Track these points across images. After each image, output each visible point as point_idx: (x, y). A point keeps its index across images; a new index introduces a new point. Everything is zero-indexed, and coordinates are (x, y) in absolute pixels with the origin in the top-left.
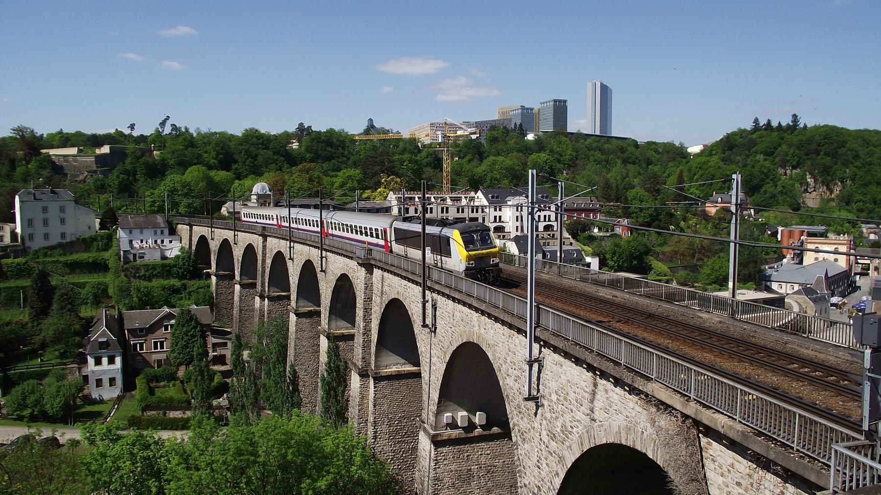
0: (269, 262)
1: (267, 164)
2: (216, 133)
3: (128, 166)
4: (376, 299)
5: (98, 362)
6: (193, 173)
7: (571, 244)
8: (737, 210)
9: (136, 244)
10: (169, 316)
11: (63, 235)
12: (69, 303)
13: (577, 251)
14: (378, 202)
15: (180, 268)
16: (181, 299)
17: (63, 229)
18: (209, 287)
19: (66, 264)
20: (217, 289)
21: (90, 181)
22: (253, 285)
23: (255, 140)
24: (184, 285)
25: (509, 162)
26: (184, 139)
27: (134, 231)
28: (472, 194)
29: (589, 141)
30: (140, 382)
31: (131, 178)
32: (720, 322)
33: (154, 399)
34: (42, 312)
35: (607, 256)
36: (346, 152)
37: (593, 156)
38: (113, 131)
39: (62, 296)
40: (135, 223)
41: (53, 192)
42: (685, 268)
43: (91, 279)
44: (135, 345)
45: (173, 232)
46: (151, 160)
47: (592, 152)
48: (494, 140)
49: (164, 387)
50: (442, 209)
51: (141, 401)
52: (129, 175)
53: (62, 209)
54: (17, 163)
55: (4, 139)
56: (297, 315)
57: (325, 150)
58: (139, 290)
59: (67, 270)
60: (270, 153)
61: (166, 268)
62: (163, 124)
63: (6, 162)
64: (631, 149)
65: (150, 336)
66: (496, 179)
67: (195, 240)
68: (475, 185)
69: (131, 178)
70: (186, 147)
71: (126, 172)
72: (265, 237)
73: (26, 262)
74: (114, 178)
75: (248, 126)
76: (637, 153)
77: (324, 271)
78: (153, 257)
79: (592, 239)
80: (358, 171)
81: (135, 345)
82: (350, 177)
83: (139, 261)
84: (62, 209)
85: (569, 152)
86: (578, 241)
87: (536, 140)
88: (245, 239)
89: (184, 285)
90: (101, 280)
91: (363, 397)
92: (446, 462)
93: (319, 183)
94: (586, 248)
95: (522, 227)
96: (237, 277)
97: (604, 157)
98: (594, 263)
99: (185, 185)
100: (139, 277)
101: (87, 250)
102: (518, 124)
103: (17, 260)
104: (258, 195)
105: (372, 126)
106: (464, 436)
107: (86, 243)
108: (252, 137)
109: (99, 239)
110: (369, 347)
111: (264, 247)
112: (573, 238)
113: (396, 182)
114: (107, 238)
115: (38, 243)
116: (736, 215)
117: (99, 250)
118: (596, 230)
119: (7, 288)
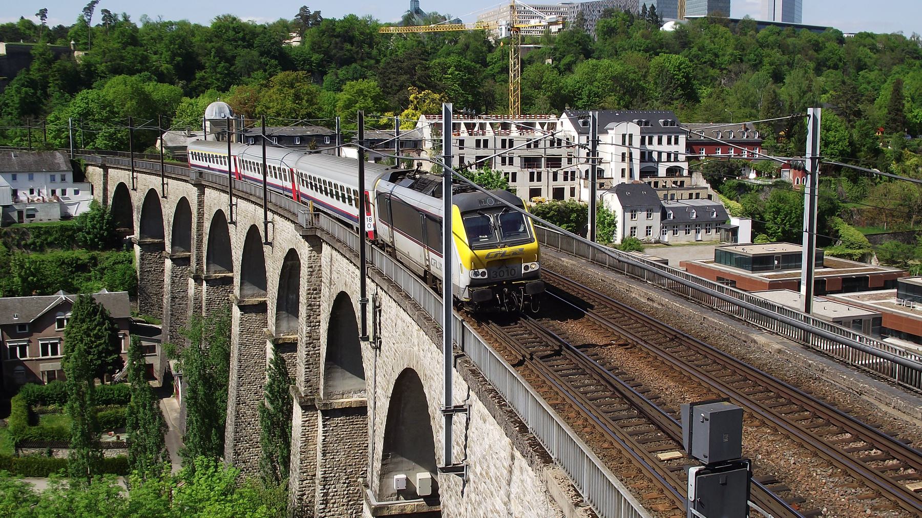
0: (207, 225)
1: (249, 71)
2: (171, 24)
3: (35, 75)
4: (325, 291)
6: (114, 88)
7: (710, 197)
8: (814, 167)
9: (23, 196)
10: (64, 306)
13: (720, 209)
14: (406, 131)
15: (88, 233)
16: (89, 279)
18: (131, 262)
20: (142, 264)
22: (186, 261)
23: (231, 33)
24: (94, 258)
25: (617, 67)
26: (122, 33)
27: (19, 176)
28: (553, 119)
29: (763, 32)
31: (39, 93)
32: (779, 351)
33: (34, 430)
35: (767, 216)
36: (375, 52)
37: (769, 56)
38: (15, 20)
42: (895, 235)
44: (13, 349)
45: (80, 177)
46: (69, 65)
47: (767, 51)
48: (609, 32)
49: (54, 412)
50: (504, 141)
51: (15, 433)
52: (35, 89)
55: (3, 27)
56: (242, 308)
57: (342, 49)
58: (22, 267)
60: (255, 53)
61: (67, 233)
62: (89, 9)
64: (832, 45)
65: (36, 335)
66: (596, 95)
67: (112, 190)
68: (560, 102)
69: (39, 93)
70: (125, 45)
71: (32, 84)
72: (201, 188)
75: (222, 12)
76: (842, 51)
77: (270, 244)
78: (49, 215)
79: (743, 189)
81: (13, 349)
82: (360, 92)
83: (26, 221)
85: (730, 51)
86: (721, 193)
87: (677, 32)
88: (178, 190)
89: (94, 258)
91: (307, 440)
93: (311, 102)
94: (733, 203)
95: (631, 170)
96: (168, 249)
97: (786, 57)
98: (744, 227)
100: (27, 246)
102: (648, 7)
104: (214, 122)
105: (418, 11)
106: (426, 509)
110: (317, 364)
111: (201, 203)
112: (713, 187)
113: (433, 100)
116: (813, 174)
118: (752, 175)
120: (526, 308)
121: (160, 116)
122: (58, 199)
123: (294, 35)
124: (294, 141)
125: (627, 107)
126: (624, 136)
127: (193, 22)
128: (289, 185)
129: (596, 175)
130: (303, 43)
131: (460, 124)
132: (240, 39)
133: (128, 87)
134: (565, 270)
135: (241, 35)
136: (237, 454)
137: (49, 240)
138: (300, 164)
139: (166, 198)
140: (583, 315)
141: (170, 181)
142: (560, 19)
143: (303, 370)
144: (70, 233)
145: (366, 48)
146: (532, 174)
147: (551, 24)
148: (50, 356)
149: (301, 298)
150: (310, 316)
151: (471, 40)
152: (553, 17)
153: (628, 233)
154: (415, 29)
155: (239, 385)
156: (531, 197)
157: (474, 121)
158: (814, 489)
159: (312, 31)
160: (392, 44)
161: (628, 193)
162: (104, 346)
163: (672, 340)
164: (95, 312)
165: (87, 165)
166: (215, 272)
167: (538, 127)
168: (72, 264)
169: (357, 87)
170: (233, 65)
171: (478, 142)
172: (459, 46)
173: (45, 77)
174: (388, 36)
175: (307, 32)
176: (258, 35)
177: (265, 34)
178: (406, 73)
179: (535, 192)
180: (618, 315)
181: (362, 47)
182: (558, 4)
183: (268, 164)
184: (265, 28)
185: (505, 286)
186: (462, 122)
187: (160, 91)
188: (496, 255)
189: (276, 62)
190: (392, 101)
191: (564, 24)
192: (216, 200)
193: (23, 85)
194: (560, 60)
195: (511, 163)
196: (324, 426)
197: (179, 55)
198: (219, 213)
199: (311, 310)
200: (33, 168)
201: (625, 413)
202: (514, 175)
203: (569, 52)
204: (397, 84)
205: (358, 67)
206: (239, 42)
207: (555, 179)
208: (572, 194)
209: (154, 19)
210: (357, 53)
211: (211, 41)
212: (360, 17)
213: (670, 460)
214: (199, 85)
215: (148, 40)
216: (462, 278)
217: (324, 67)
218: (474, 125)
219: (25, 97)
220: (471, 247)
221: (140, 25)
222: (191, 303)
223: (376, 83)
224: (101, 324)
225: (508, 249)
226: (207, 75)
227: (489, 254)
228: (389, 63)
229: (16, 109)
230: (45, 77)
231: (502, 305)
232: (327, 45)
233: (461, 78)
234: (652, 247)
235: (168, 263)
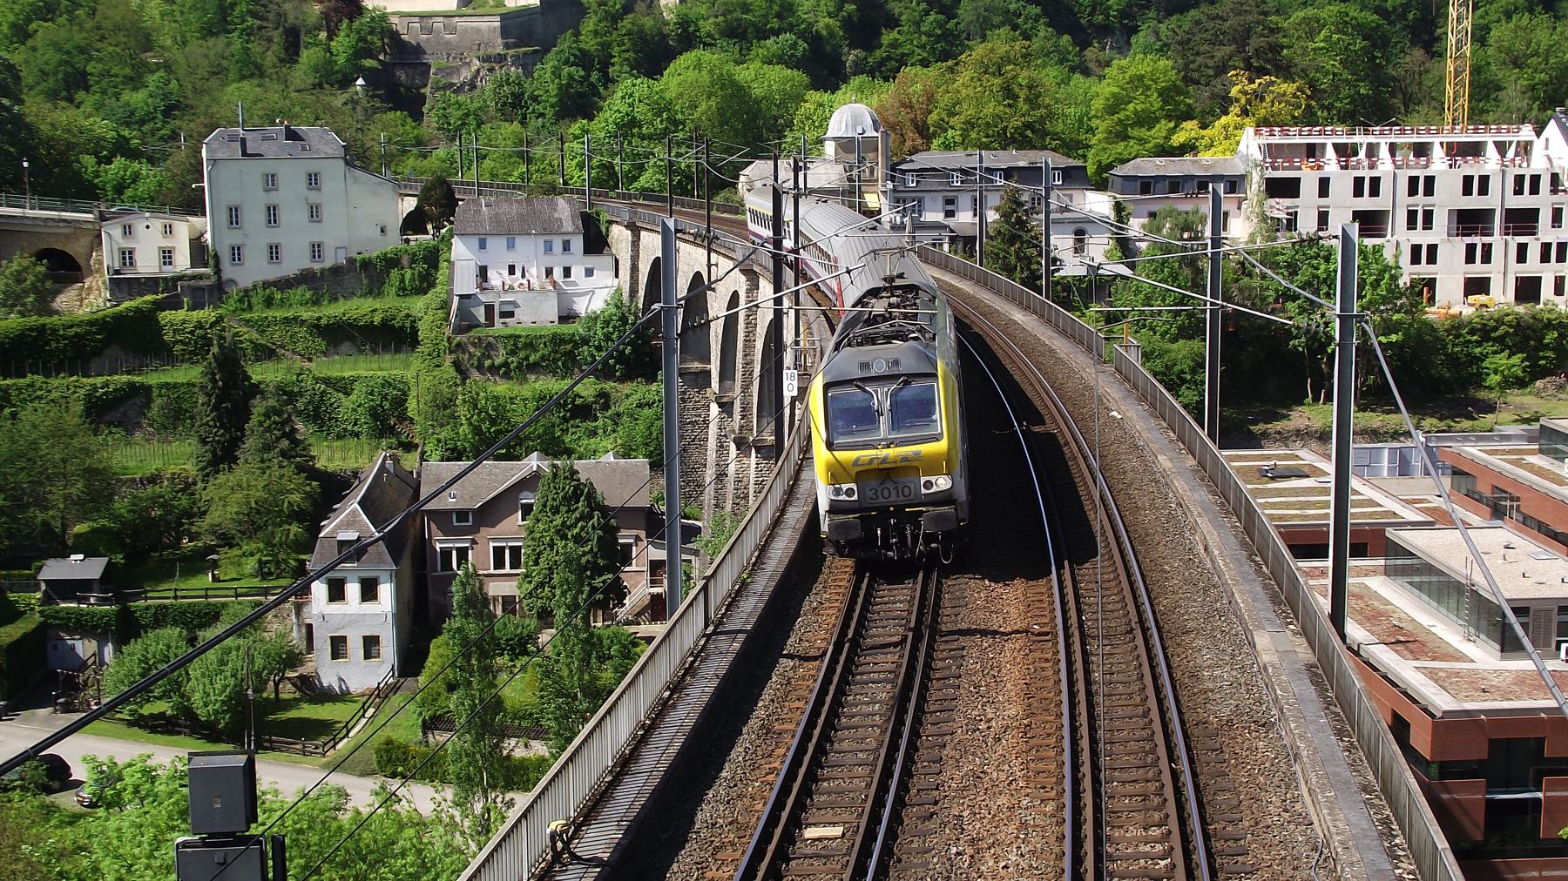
3: (589, 43)
5: (337, 593)
9: (495, 279)
11: (316, 250)
12: (285, 435)
14: (1206, 161)
15: (599, 349)
16: (594, 433)
17: (315, 233)
19: (317, 326)
21: (487, 85)
24: (604, 396)
27: (490, 241)
28: (1527, 132)
30: (440, 651)
31: (595, 76)
34: (222, 456)
39: (267, 415)
40: (496, 219)
41: (292, 135)
43: (368, 370)
44: (446, 554)
45: (596, 243)
46: (648, 22)
50: (1413, 181)
52: (588, 68)
53: (313, 180)
54: (304, 39)
59: (321, 343)
61: (561, 351)
63: (277, 36)
65: (485, 532)
69: (595, 76)
71: (583, 59)
73: (220, 319)
74: (547, 79)
78: (536, 315)
81: (446, 554)
84: (313, 180)
89: (604, 396)
90: (397, 372)
93: (1033, 102)
99: (661, 107)
100: (493, 369)
101: (375, 290)
103: (197, 315)
104: (845, 145)
107: (371, 273)
109: (405, 260)
114: (425, 260)
115: (252, 271)
117: (403, 291)
119: (166, 385)
122: (554, 283)
131: (1324, 145)
133: (705, 73)
137: (532, 359)
144: (569, 347)
146: (1471, 249)
148: (507, 570)
156: (1466, 295)
157: (1357, 139)
162: (589, 557)
164: (576, 496)
165: (610, 222)
167: (1491, 151)
168: (566, 404)
169: (1132, 71)
171: (1358, 182)
173: (606, 46)
179: (1476, 286)
185: (893, 515)
188: (872, 460)
189: (1038, 10)
190: (1197, 97)
193: (567, 62)
195: (1428, 224)
200: (516, 227)
202: (1432, 249)
204: (1211, 63)
213: (820, 839)
214: (889, 58)
217: (1133, 17)
219: (569, 85)
223: (1170, 63)
224: (586, 517)
225: (893, 452)
226: (902, 39)
227: (857, 460)
228: (1198, 23)
229: (552, 106)
230: (606, 46)
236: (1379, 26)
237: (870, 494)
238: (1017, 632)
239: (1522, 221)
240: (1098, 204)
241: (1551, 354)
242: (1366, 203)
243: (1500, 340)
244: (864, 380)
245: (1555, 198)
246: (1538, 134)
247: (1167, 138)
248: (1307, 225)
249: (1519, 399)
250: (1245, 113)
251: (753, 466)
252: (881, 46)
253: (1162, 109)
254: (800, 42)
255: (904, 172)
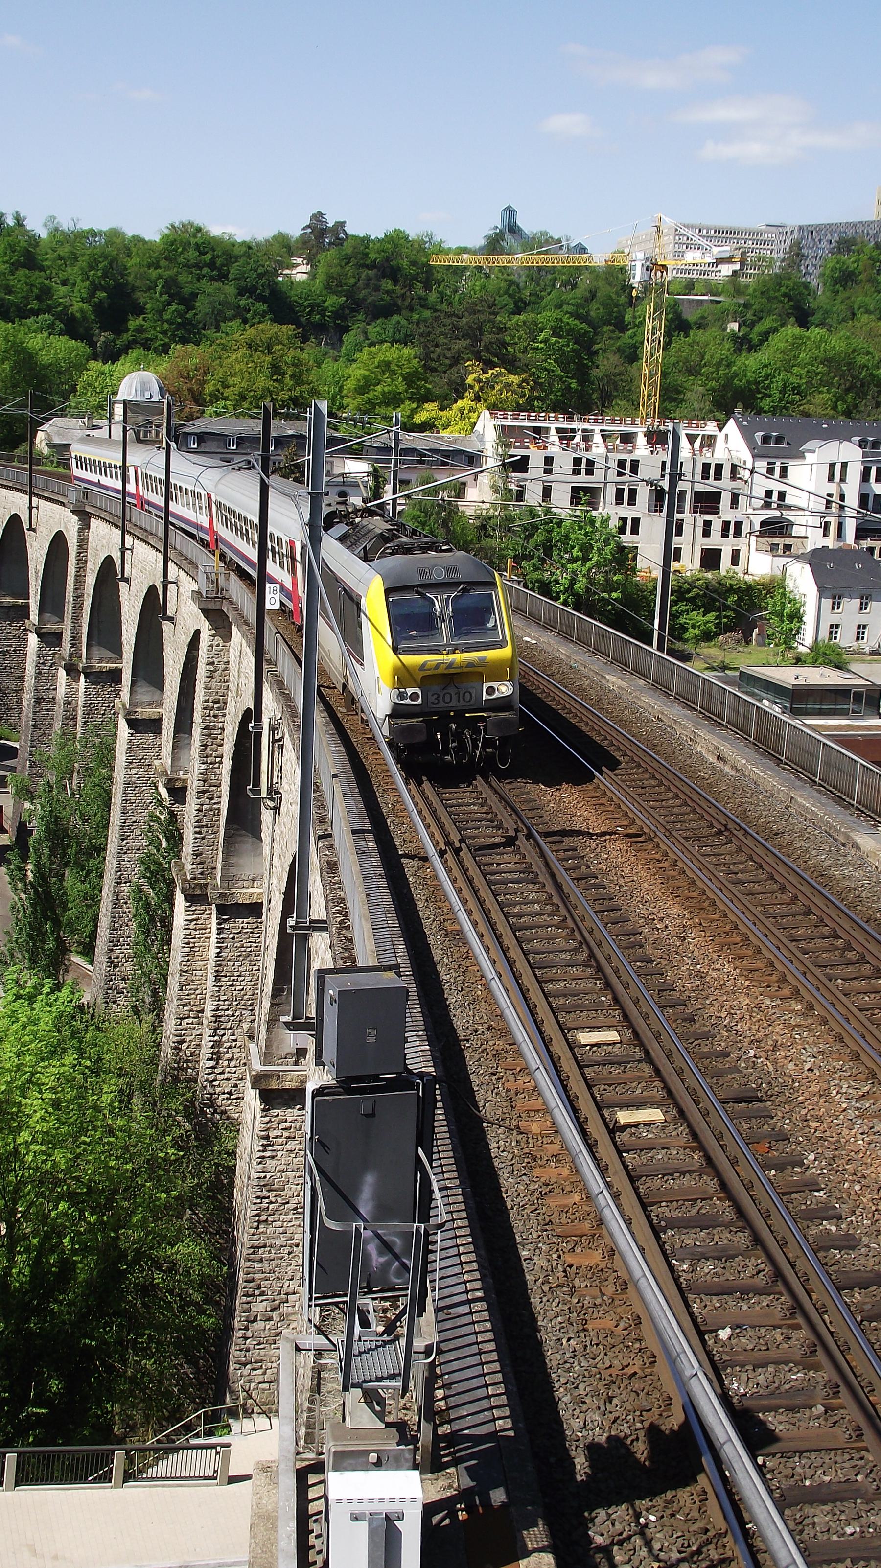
0: (90, 580)
1: (218, 319)
2: (93, 233)
14: (449, 437)
23: (192, 254)
28: (711, 428)
36: (433, 297)
50: (622, 464)
56: (131, 724)
57: (377, 289)
60: (230, 289)
66: (797, 390)
68: (732, 399)
70: (15, 267)
72: (84, 517)
75: (179, 217)
80: (407, 351)
82: (386, 366)
88: (52, 518)
92: (291, 1145)
93: (298, 379)
95: (840, 526)
96: (34, 616)
104: (126, 403)
105: (513, 229)
108: (186, 246)
111: (83, 544)
113: (508, 386)
120: (488, 759)
121: (46, 391)
123: (299, 261)
124: (226, 444)
125: (848, 414)
126: (832, 466)
127: (130, 232)
128: (204, 521)
129: (776, 529)
130: (312, 275)
131: (547, 430)
132: (206, 265)
134: (604, 699)
135: (208, 257)
136: (113, 964)
138: (220, 486)
139: (34, 530)
140: (590, 778)
141: (42, 502)
142: (738, 254)
143: (192, 836)
145: (419, 290)
147: (720, 261)
149: (195, 714)
150: (205, 746)
151: (601, 283)
152: (725, 250)
153: (824, 634)
154: (503, 260)
155: (121, 852)
157: (574, 425)
158: (819, 1119)
159: (329, 256)
160: (465, 285)
161: (830, 565)
163: (720, 833)
166: (101, 661)
169: (381, 357)
170: (193, 308)
171: (577, 462)
172: (578, 292)
174: (458, 271)
175: (321, 257)
176: (237, 258)
177: (249, 257)
178: (466, 336)
180: (653, 782)
181: (411, 287)
182: (760, 225)
183: (172, 481)
184: (250, 248)
186: (553, 426)
187: (54, 348)
188: (438, 665)
189: (265, 307)
190: (437, 383)
191: (743, 263)
192: (104, 539)
194: (752, 325)
195: (632, 501)
196: (220, 931)
197: (104, 289)
198: (109, 560)
199: (209, 735)
201: (566, 956)
202: (636, 522)
203: (769, 312)
205: (404, 322)
206: (205, 270)
207: (706, 533)
208: (735, 560)
209: (66, 225)
210: (403, 296)
211: (158, 267)
212: (412, 236)
213: (598, 1045)
215: (54, 261)
216: (379, 700)
217: (344, 318)
218: (573, 431)
220: (395, 650)
221: (44, 234)
222: (59, 710)
223: (412, 352)
225: (459, 657)
226: (146, 325)
227: (425, 664)
231: (446, 751)
232: (353, 281)
233: (560, 349)
234: (864, 661)
235: (33, 640)
236: (586, 332)
237: (432, 699)
238: (590, 835)
239: (707, 502)
240: (357, 468)
241: (731, 614)
242: (582, 480)
243: (692, 600)
244: (421, 586)
245: (734, 484)
246: (720, 429)
247: (411, 417)
248: (533, 497)
249: (706, 651)
250: (477, 399)
251: (82, 690)
252: (127, 330)
253: (406, 391)
254: (57, 322)
255: (187, 434)
